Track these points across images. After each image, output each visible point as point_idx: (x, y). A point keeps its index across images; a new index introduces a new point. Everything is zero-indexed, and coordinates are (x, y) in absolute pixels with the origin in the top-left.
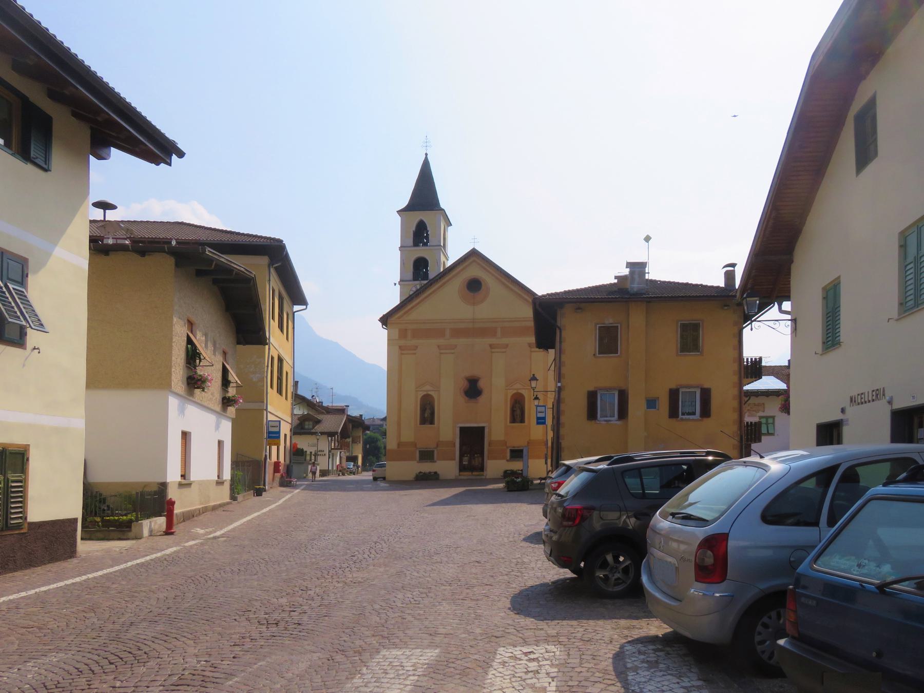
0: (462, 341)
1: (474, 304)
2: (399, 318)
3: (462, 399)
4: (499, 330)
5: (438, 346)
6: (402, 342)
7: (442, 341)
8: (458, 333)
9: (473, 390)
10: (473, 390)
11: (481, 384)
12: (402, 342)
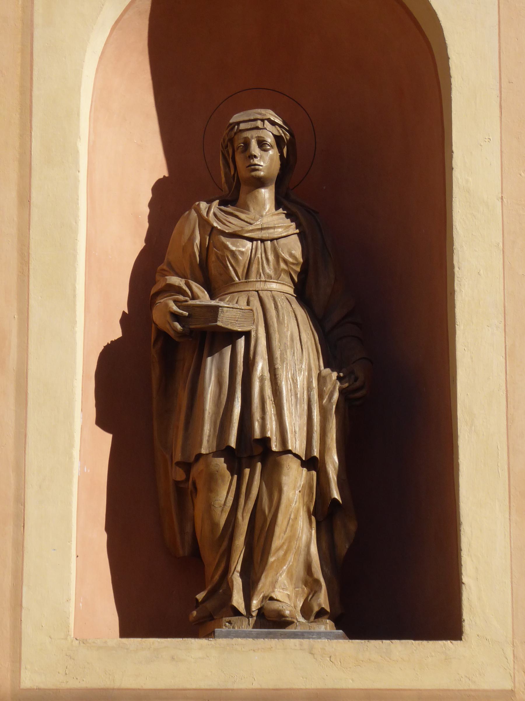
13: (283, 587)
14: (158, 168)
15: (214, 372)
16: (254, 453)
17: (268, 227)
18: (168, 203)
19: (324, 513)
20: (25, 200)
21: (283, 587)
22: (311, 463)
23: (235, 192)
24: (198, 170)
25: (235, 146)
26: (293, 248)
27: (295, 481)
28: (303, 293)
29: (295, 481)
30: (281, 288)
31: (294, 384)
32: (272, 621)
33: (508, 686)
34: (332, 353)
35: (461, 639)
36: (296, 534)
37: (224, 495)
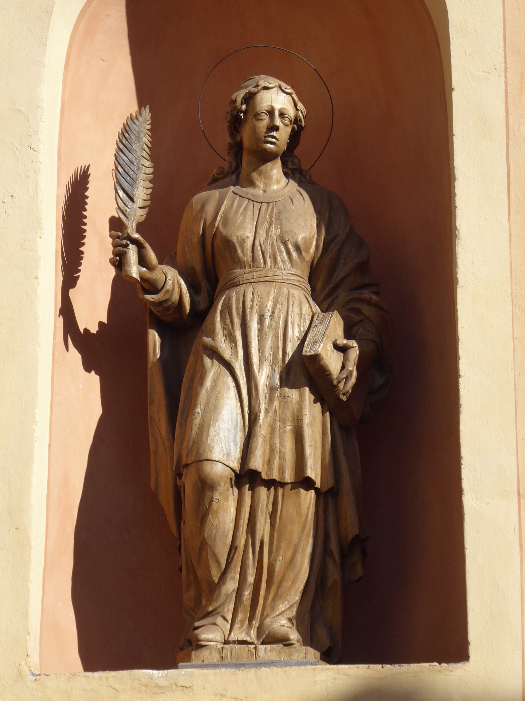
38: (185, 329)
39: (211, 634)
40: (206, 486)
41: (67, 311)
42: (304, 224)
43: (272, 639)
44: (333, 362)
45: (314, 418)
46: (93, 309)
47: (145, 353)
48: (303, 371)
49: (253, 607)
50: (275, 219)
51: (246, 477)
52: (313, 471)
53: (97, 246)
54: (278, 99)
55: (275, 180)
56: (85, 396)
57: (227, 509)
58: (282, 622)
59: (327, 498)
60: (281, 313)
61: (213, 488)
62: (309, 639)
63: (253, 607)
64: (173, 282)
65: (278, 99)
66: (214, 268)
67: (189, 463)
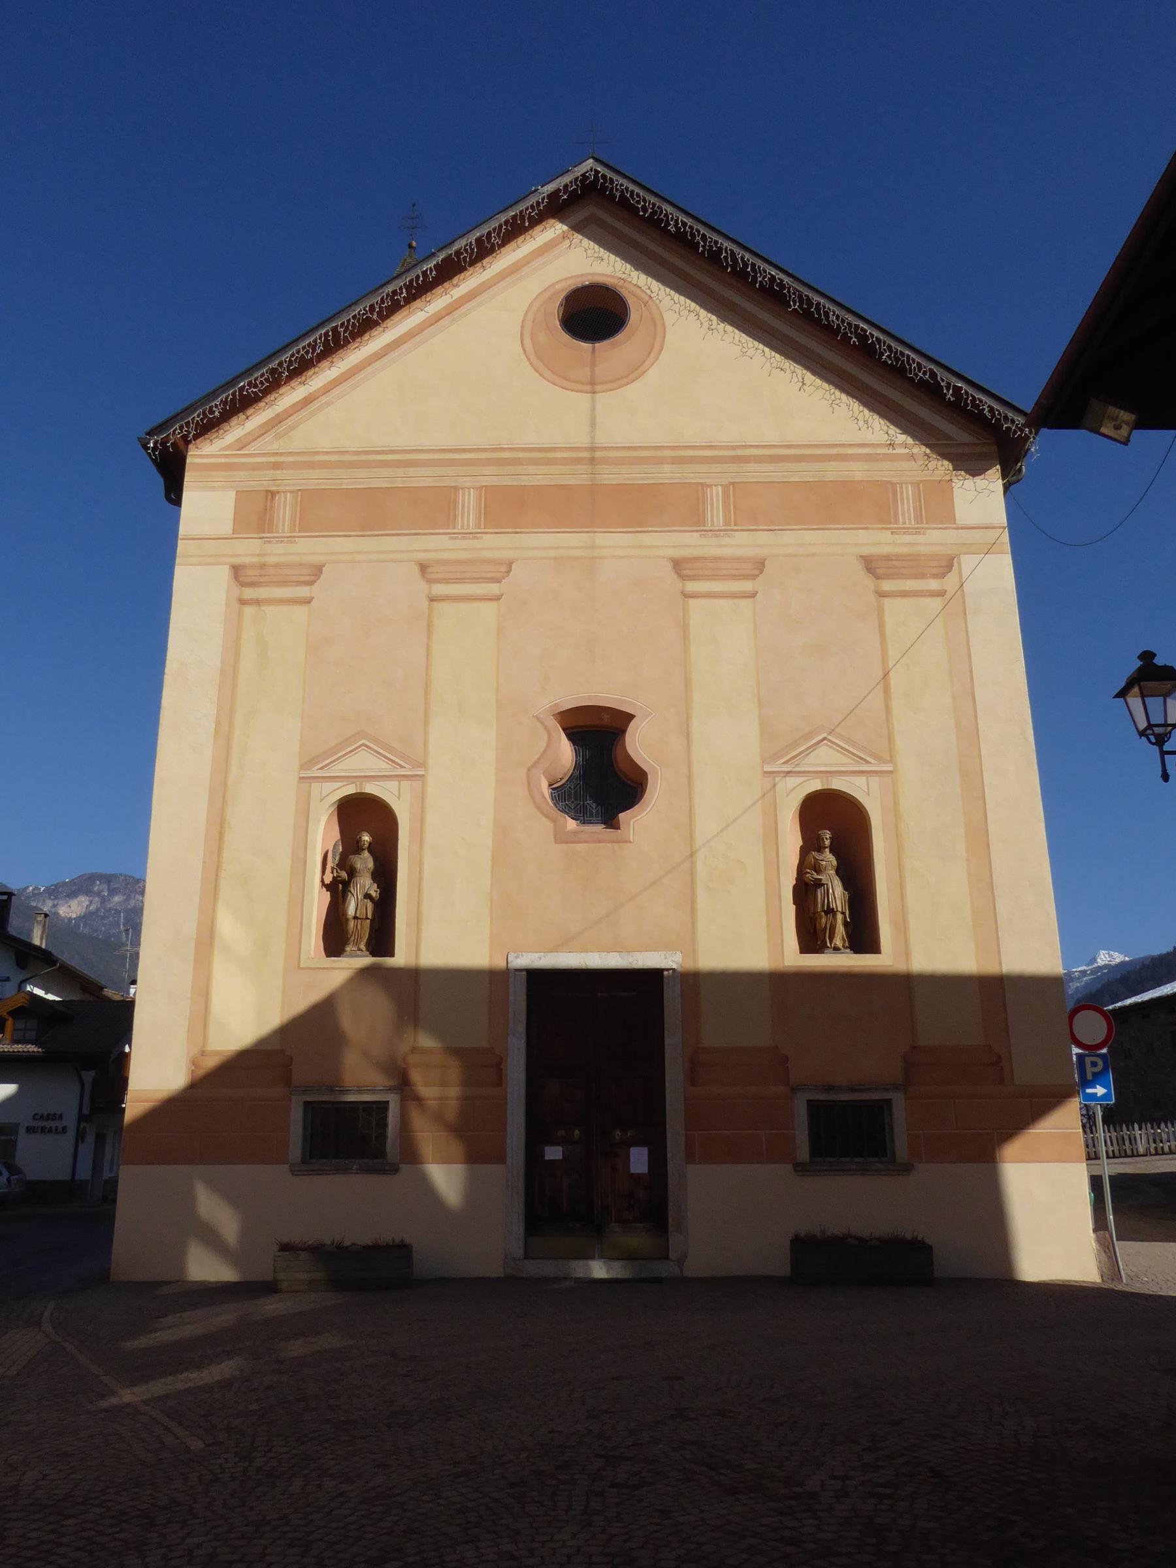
0: (537, 544)
1: (592, 385)
2: (242, 444)
3: (543, 830)
4: (716, 495)
5: (423, 568)
6: (248, 550)
7: (437, 545)
8: (512, 506)
9: (601, 774)
10: (601, 774)
11: (639, 744)
12: (248, 550)
13: (838, 942)
14: (800, 842)
15: (820, 892)
16: (830, 911)
17: (828, 859)
18: (804, 852)
19: (846, 924)
20: (778, 854)
21: (838, 942)
22: (843, 913)
23: (820, 849)
24: (810, 844)
25: (820, 839)
26: (835, 863)
27: (840, 917)
28: (837, 873)
29: (840, 917)
30: (833, 872)
31: (837, 893)
32: (836, 949)
33: (233, 494)
34: (845, 887)
35: (630, 717)
36: (840, 929)
37: (824, 921)
38: (346, 884)
39: (348, 949)
40: (347, 920)
41: (322, 881)
42: (370, 864)
43: (360, 950)
44: (374, 894)
45: (370, 905)
46: (328, 879)
47: (338, 890)
48: (367, 896)
49: (357, 943)
50: (365, 862)
51: (355, 918)
52: (370, 916)
53: (330, 865)
54: (366, 838)
55: (366, 854)
56: (327, 896)
57: (352, 924)
58: (362, 947)
59: (372, 921)
60: (365, 884)
61: (582, 815)
62: (368, 950)
63: (357, 943)
64: (344, 875)
65: (366, 838)
66: (352, 872)
67: (345, 914)
